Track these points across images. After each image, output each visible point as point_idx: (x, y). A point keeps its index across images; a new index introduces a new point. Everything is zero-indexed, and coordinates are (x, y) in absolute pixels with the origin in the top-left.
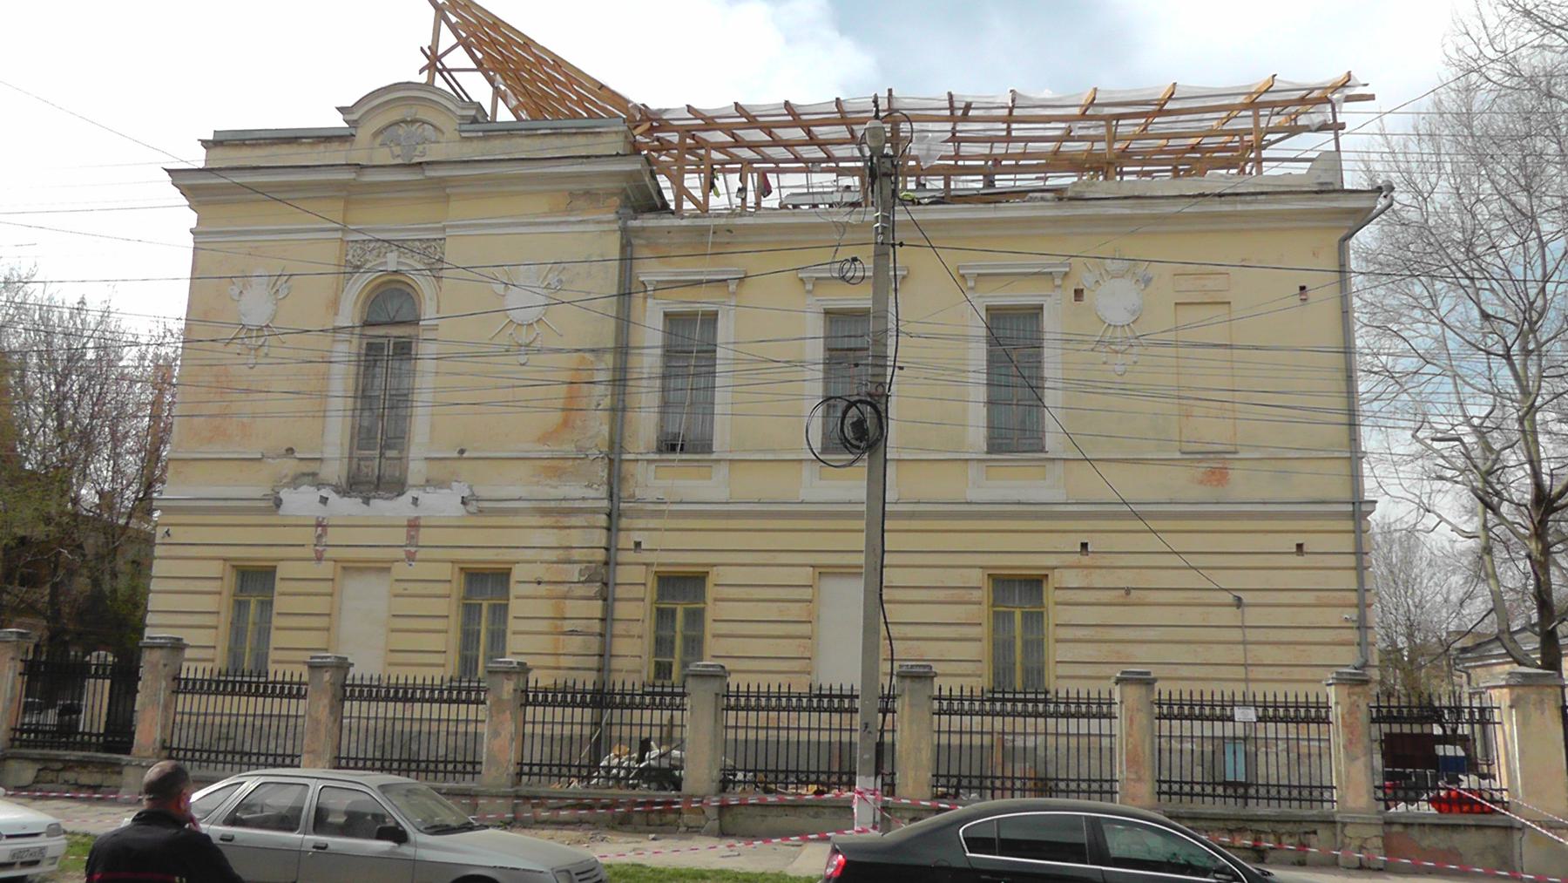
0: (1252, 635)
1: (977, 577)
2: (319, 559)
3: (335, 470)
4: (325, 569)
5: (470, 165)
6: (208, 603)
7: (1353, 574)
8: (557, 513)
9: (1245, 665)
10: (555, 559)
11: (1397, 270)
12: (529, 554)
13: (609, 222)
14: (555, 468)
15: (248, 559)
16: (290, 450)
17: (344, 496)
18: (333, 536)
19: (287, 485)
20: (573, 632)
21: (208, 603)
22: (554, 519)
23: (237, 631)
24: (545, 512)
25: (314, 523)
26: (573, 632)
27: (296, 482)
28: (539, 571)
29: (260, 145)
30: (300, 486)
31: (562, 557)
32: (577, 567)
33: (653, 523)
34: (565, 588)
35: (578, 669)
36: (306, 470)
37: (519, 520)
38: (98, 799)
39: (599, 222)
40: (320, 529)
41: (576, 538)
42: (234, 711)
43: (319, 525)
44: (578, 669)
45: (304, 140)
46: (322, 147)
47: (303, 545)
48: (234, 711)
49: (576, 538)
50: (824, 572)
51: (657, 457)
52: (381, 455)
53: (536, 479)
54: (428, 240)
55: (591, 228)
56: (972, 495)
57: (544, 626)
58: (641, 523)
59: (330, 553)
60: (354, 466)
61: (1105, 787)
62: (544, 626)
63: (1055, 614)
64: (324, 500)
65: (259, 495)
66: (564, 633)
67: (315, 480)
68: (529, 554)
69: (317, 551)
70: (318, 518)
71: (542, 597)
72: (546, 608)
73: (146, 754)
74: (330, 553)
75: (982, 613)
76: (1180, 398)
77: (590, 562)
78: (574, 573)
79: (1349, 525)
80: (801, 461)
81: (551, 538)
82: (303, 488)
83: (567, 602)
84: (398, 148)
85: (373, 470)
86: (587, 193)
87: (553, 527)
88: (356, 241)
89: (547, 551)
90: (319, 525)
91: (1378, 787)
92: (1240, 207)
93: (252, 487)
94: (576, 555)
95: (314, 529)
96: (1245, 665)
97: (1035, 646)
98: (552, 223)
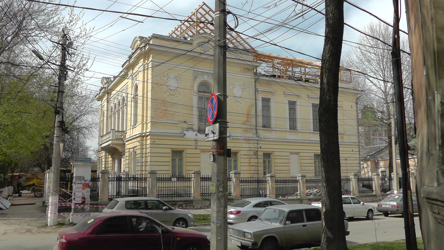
0: (348, 165)
1: (169, 151)
2: (196, 149)
3: (196, 127)
4: (198, 151)
5: (229, 59)
6: (277, 161)
7: (358, 155)
8: (248, 140)
9: (347, 170)
10: (248, 150)
11: (55, 84)
12: (243, 149)
13: (253, 76)
14: (246, 130)
15: (178, 148)
16: (185, 122)
17: (201, 134)
18: (199, 143)
19: (186, 130)
20: (253, 166)
21: (277, 161)
22: (247, 141)
23: (173, 167)
24: (245, 140)
25: (194, 140)
26: (253, 166)
27: (188, 129)
28: (245, 153)
29: (168, 40)
30: (189, 131)
31: (249, 150)
32: (253, 152)
33: (263, 143)
34: (251, 156)
35: (254, 173)
36: (190, 127)
37: (240, 141)
38: (192, 208)
39: (250, 76)
40: (196, 142)
41: (252, 145)
42: (206, 185)
43: (195, 141)
44: (254, 173)
45: (181, 42)
46: (185, 45)
47: (191, 145)
48: (180, 186)
49: (252, 145)
50: (291, 153)
51: (262, 128)
52: (205, 124)
53: (242, 132)
54: (197, 71)
55: (249, 77)
56: (287, 138)
57: (247, 164)
58: (261, 143)
59: (199, 147)
60: (199, 126)
61: (189, 195)
62: (247, 164)
63: (185, 160)
64: (196, 135)
65: (179, 132)
66: (251, 166)
67: (192, 129)
68: (243, 149)
69: (195, 147)
70: (195, 139)
71: (246, 158)
72: (247, 160)
73: (238, 197)
74: (199, 147)
75: (170, 159)
76: (275, 120)
77: (254, 151)
78: (252, 153)
79: (358, 147)
80: (310, 133)
81: (247, 145)
82: (190, 131)
83: (251, 159)
84: (202, 48)
85: (203, 127)
86: (247, 68)
87: (247, 143)
88: (196, 71)
89: (246, 148)
90: (195, 141)
91: (201, 194)
92: (346, 90)
93: (176, 130)
94: (252, 149)
95: (194, 142)
96: (347, 170)
97: (181, 166)
98: (241, 74)
